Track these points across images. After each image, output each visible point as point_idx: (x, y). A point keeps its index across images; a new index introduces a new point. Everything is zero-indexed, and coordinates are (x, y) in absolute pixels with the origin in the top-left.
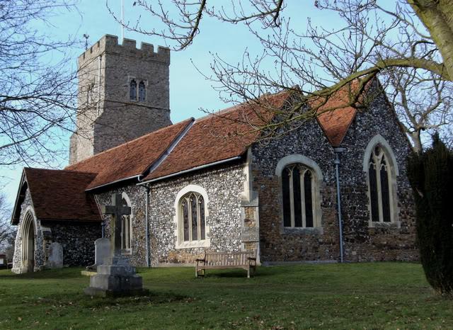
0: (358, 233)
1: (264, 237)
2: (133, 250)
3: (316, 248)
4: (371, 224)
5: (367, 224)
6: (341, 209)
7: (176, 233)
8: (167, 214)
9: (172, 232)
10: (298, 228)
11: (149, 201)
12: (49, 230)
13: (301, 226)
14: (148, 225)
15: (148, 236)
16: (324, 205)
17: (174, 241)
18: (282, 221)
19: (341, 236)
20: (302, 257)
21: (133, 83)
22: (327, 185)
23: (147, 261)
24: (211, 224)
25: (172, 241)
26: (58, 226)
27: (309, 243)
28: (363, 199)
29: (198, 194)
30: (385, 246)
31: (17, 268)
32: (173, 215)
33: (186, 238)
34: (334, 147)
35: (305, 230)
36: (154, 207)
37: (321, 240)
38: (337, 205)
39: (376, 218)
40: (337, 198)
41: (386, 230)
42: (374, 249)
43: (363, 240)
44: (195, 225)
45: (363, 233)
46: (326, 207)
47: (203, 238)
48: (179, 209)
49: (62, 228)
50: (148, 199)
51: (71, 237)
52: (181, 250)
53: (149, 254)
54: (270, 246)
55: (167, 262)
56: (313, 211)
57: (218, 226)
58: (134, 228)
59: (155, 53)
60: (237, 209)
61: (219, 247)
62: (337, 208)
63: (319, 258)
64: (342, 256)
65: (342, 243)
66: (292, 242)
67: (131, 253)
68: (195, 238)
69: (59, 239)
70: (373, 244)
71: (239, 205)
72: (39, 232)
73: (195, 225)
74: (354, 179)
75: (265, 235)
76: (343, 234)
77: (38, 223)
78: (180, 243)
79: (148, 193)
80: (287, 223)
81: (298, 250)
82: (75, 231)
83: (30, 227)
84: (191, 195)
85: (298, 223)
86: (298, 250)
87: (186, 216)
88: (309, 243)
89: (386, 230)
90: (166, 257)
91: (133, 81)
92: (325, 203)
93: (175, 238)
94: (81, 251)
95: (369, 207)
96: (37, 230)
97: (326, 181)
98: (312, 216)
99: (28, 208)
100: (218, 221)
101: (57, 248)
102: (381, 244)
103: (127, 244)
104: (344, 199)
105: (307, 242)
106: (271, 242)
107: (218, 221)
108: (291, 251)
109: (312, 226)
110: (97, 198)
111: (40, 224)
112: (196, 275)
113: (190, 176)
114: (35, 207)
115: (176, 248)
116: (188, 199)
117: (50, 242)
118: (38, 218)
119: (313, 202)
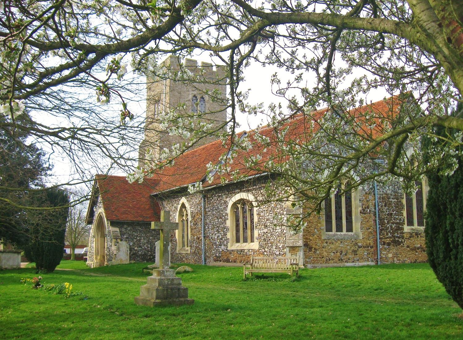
0: (394, 237)
1: (307, 242)
2: (191, 249)
3: (355, 252)
4: (407, 229)
5: (403, 229)
6: (379, 215)
7: (229, 235)
8: (221, 218)
9: (225, 235)
10: (339, 233)
11: (205, 206)
12: (117, 229)
13: (342, 231)
14: (204, 227)
15: (204, 237)
16: (363, 212)
17: (227, 243)
18: (324, 227)
19: (379, 240)
20: (342, 260)
21: (194, 98)
22: (366, 193)
23: (203, 259)
24: (260, 229)
25: (225, 243)
26: (125, 226)
27: (349, 247)
28: (399, 206)
29: (248, 201)
30: (418, 248)
31: (91, 262)
32: (225, 220)
33: (238, 241)
34: (372, 159)
35: (345, 235)
36: (209, 211)
37: (360, 244)
38: (375, 212)
39: (410, 223)
40: (375, 206)
41: (420, 234)
42: (409, 251)
43: (398, 243)
44: (245, 228)
45: (399, 238)
46: (365, 214)
47: (252, 241)
48: (231, 214)
49: (129, 228)
50: (205, 204)
51: (137, 236)
52: (232, 250)
53: (205, 253)
54: (313, 250)
55: (220, 261)
56: (353, 217)
57: (265, 231)
58: (192, 229)
59: (214, 72)
60: (283, 216)
61: (266, 249)
62: (375, 215)
63: (358, 260)
64: (379, 258)
65: (380, 247)
66: (332, 246)
67: (189, 252)
68: (245, 241)
69: (126, 238)
70: (408, 247)
71: (285, 213)
72: (109, 232)
73: (245, 228)
74: (390, 187)
75: (308, 240)
76: (380, 238)
77: (108, 223)
78: (231, 246)
79: (204, 199)
80: (329, 229)
81: (338, 253)
82: (140, 232)
83: (100, 226)
84: (243, 202)
85: (339, 229)
86: (338, 253)
87: (237, 221)
88: (349, 247)
89: (420, 234)
90: (220, 257)
91: (195, 96)
92: (364, 210)
93: (227, 239)
94: (145, 249)
95: (405, 213)
96: (107, 230)
97: (365, 191)
98: (352, 222)
99: (100, 210)
100: (266, 226)
101: (124, 246)
102: (415, 247)
103: (186, 244)
104: (382, 206)
105: (348, 247)
106: (314, 246)
107: (266, 226)
108: (332, 254)
109: (351, 231)
110: (398, 7)
111: (109, 224)
112: (244, 277)
113: (240, 186)
114: (105, 209)
115: (229, 249)
116: (239, 206)
117: (119, 240)
118: (107, 220)
119: (353, 209)
